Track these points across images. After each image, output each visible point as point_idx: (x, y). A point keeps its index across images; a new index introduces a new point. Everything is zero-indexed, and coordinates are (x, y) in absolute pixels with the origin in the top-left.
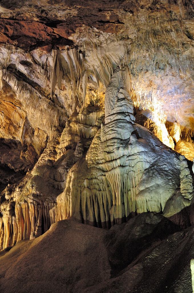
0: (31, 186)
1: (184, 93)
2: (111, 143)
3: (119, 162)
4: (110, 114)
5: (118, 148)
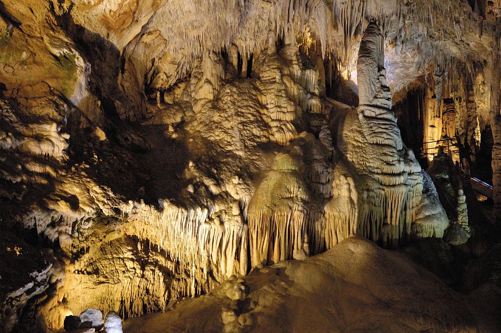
1: (392, 73)
2: (389, 152)
3: (402, 179)
4: (371, 102)
5: (399, 161)
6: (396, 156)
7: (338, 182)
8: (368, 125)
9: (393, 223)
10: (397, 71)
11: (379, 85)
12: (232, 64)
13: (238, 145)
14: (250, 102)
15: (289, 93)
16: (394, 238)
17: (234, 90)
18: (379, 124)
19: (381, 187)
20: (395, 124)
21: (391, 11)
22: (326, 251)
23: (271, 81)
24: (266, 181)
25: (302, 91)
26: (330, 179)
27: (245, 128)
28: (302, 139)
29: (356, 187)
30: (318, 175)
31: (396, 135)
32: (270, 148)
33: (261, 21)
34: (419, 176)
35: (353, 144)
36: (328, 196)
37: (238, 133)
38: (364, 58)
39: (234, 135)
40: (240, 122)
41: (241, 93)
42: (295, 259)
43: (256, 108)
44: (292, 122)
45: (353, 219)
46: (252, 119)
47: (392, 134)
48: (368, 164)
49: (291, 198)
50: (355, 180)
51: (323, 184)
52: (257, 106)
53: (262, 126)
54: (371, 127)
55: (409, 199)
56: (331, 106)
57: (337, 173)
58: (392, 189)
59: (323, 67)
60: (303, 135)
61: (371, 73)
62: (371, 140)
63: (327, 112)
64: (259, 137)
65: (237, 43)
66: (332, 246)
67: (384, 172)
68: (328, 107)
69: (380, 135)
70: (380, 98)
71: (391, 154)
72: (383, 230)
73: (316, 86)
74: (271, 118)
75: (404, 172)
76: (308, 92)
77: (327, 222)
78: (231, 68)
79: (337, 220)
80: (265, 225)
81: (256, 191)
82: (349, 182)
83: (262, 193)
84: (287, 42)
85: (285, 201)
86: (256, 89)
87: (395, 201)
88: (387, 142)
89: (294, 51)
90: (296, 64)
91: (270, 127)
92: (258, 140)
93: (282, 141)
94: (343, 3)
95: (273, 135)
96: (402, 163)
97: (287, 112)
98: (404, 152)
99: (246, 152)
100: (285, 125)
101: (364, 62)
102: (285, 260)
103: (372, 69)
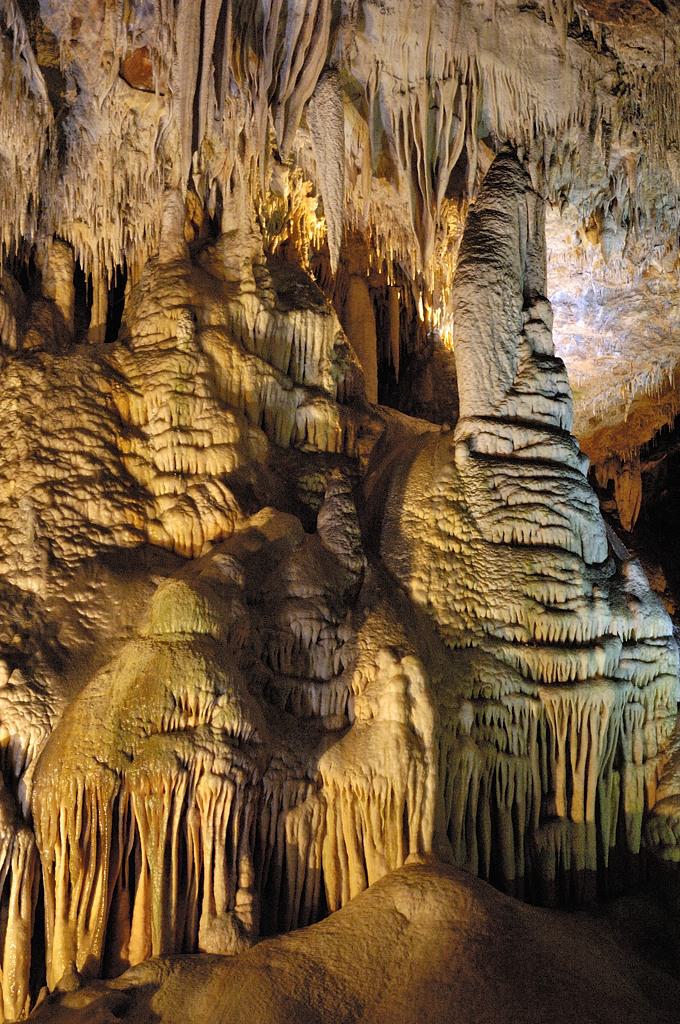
0: (211, 690)
2: (555, 569)
3: (600, 661)
4: (497, 408)
5: (591, 600)
6: (579, 582)
7: (368, 672)
8: (485, 481)
9: (577, 815)
10: (629, 321)
11: (524, 353)
12: (51, 301)
13: (27, 555)
14: (85, 417)
15: (223, 384)
16: (580, 866)
17: (36, 378)
18: (522, 478)
19: (527, 689)
20: (578, 478)
21: (563, 114)
22: (328, 915)
23: (162, 347)
24: (104, 676)
25: (271, 379)
26: (345, 663)
27: (58, 500)
28: (253, 533)
29: (433, 691)
30: (300, 652)
31: (578, 514)
32: (140, 563)
33: (132, 155)
34: (664, 650)
35: (431, 548)
36: (336, 723)
37: (30, 518)
38: (473, 266)
39: (18, 525)
40: (41, 480)
41: (55, 388)
42: (204, 952)
43: (105, 434)
44: (227, 480)
45: (419, 799)
46: (87, 469)
47: (564, 510)
48: (481, 612)
49: (188, 733)
50: (427, 666)
51: (319, 681)
52: (106, 427)
53: (123, 494)
54: (495, 489)
55: (630, 728)
56: (377, 427)
57: (366, 644)
58: (566, 695)
59: (371, 312)
60: (258, 520)
61: (497, 314)
62: (493, 530)
63: (365, 447)
64: (105, 531)
65: (73, 237)
66: (349, 898)
67: (538, 637)
68: (370, 432)
69: (524, 515)
70: (529, 394)
71: (562, 577)
72: (539, 839)
73: (324, 364)
74: (155, 467)
75: (609, 637)
76: (296, 385)
77: (330, 812)
78: (46, 315)
79: (362, 805)
80: (94, 831)
81: (67, 710)
82: (408, 672)
83: (87, 718)
84: (228, 224)
85: (164, 743)
86: (114, 374)
87: (579, 735)
88: (547, 537)
89: (248, 253)
90: (249, 293)
91: (150, 497)
92: (102, 539)
93: (188, 544)
94: (403, 93)
95: (158, 522)
96: (601, 607)
97: (213, 445)
98: (609, 572)
99: (51, 580)
100: (201, 488)
101: (472, 279)
102: (163, 955)
103: (499, 300)
